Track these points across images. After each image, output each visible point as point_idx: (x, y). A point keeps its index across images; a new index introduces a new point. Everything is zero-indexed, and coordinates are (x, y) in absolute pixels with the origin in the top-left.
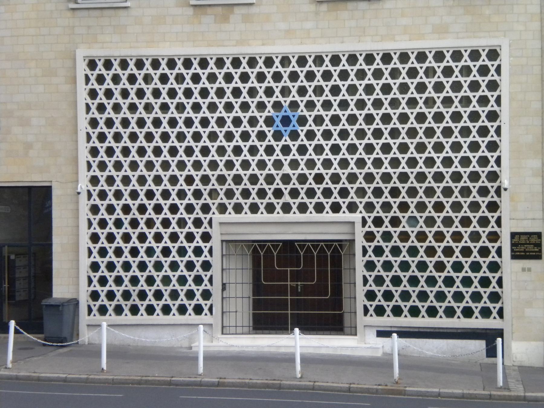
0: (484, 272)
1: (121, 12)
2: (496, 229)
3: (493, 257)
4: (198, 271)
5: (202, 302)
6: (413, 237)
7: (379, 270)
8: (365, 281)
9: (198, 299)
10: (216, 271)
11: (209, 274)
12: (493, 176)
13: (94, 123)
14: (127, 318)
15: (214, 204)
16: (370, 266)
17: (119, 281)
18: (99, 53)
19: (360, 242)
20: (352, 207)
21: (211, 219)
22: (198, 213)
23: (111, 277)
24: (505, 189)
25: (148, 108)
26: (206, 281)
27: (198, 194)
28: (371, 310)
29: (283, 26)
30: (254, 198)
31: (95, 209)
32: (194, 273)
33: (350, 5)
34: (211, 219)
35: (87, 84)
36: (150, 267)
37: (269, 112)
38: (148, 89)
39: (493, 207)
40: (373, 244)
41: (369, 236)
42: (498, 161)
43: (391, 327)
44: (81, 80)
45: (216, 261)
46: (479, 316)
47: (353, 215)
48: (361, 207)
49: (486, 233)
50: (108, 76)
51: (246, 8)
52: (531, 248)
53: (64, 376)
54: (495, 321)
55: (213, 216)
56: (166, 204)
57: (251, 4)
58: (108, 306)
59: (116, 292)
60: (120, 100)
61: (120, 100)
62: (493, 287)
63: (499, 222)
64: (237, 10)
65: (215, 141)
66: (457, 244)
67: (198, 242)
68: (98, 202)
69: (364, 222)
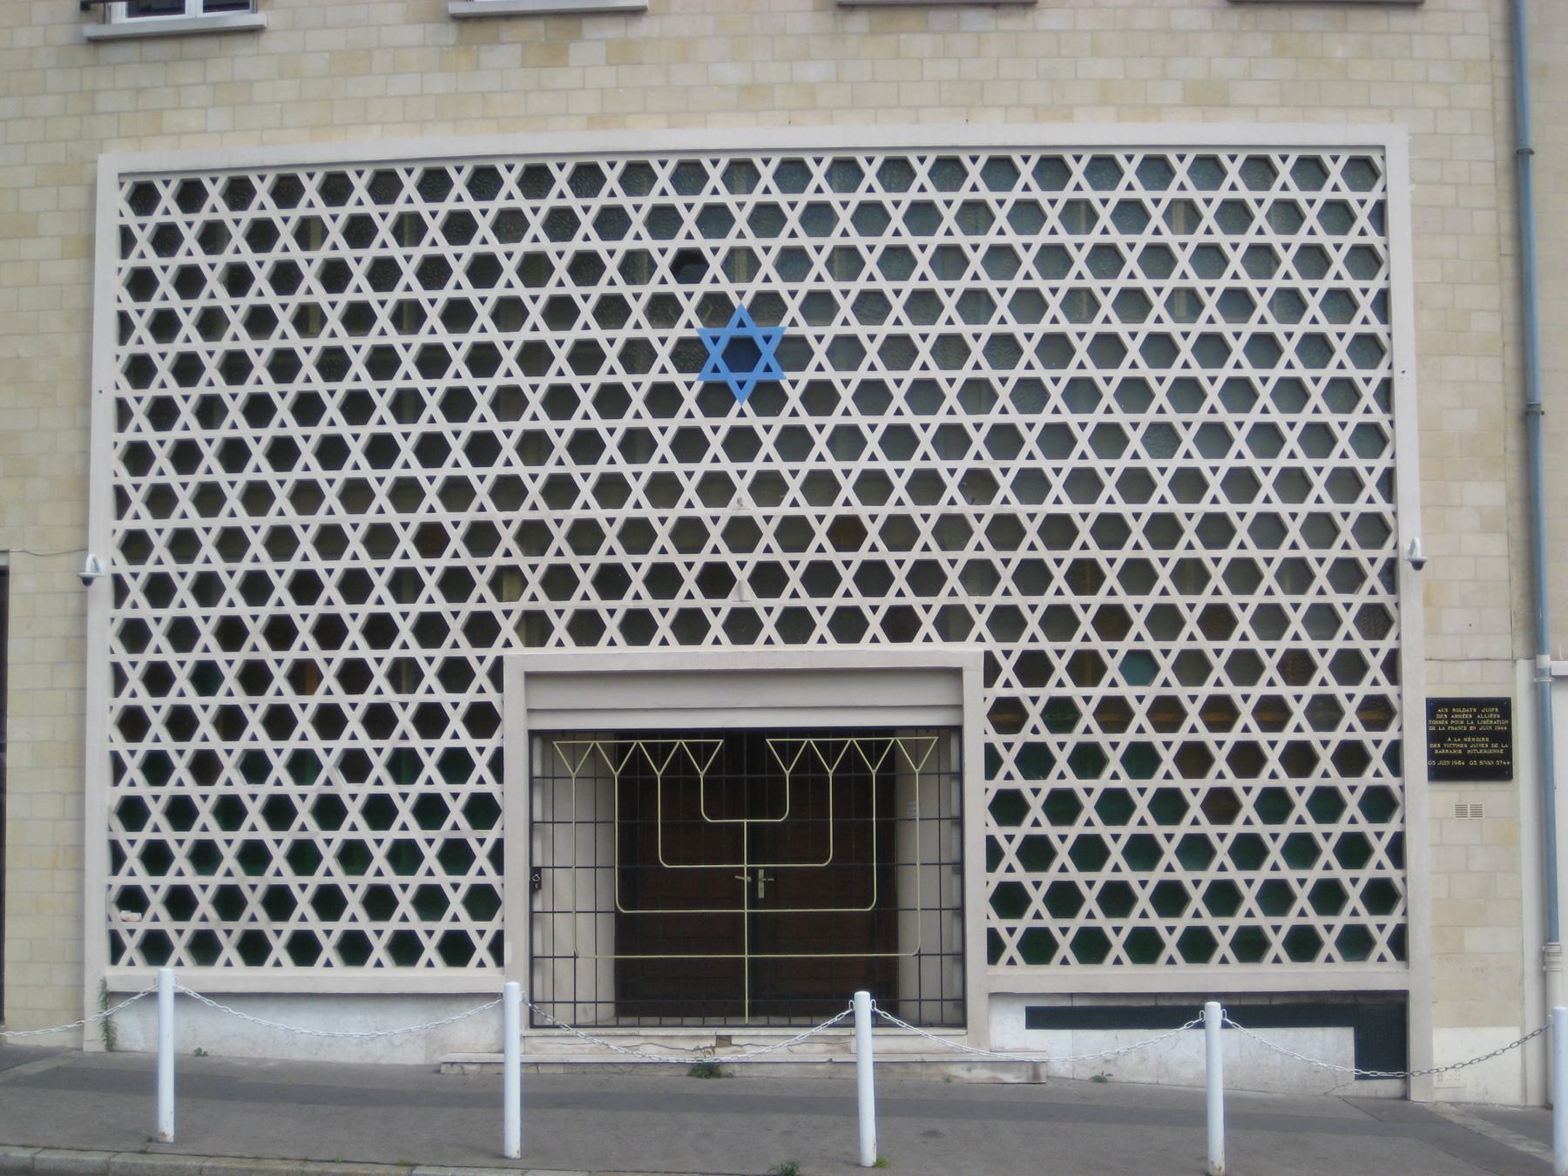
0: (1352, 819)
1: (242, 47)
2: (1385, 688)
3: (1375, 773)
4: (455, 827)
5: (468, 925)
6: (1140, 716)
7: (1038, 821)
8: (994, 854)
9: (457, 916)
10: (512, 825)
11: (491, 836)
12: (1375, 529)
13: (140, 371)
14: (231, 972)
15: (507, 613)
16: (1008, 807)
17: (205, 856)
18: (166, 158)
19: (978, 732)
20: (953, 624)
21: (499, 662)
22: (457, 644)
23: (180, 844)
24: (1418, 565)
25: (308, 320)
26: (482, 859)
27: (456, 584)
28: (1011, 945)
29: (732, 73)
30: (637, 595)
31: (135, 635)
32: (441, 835)
33: (939, 18)
34: (499, 662)
35: (125, 254)
36: (304, 814)
37: (689, 325)
38: (309, 262)
39: (1376, 621)
40: (1019, 739)
41: (1007, 715)
42: (1388, 483)
43: (1072, 995)
44: (107, 242)
45: (513, 795)
46: (1336, 954)
47: (954, 647)
48: (980, 623)
49: (1357, 701)
50: (190, 227)
51: (621, 21)
52: (1482, 746)
53: (25, 1154)
54: (1382, 967)
55: (507, 653)
56: (355, 616)
57: (636, 12)
58: (173, 936)
59: (197, 892)
60: (224, 300)
61: (224, 300)
62: (1378, 866)
63: (1392, 666)
64: (590, 28)
65: (593, 551)
66: (1272, 736)
67: (456, 734)
68: (146, 612)
69: (991, 670)
